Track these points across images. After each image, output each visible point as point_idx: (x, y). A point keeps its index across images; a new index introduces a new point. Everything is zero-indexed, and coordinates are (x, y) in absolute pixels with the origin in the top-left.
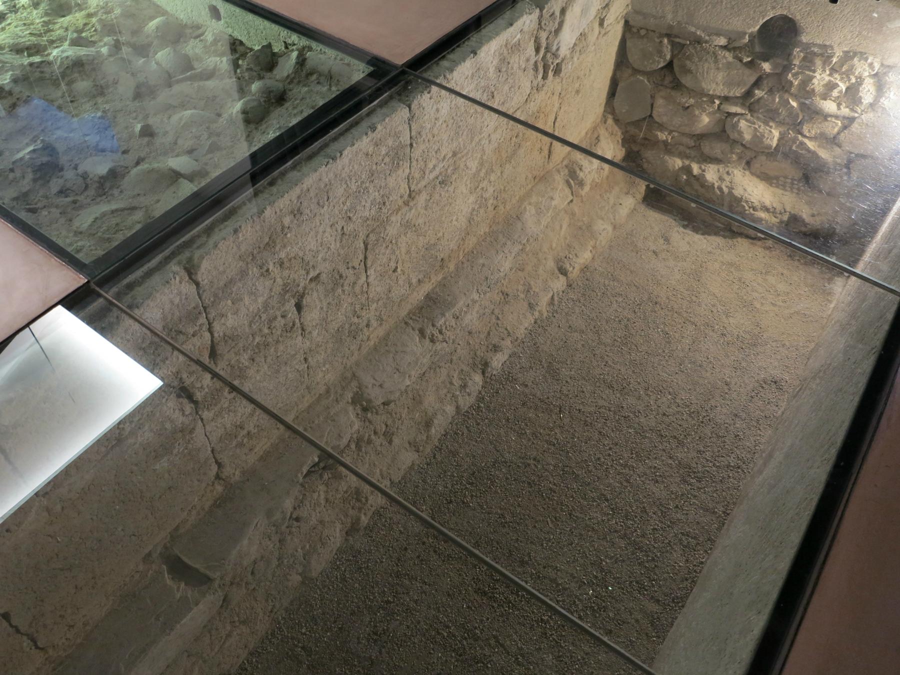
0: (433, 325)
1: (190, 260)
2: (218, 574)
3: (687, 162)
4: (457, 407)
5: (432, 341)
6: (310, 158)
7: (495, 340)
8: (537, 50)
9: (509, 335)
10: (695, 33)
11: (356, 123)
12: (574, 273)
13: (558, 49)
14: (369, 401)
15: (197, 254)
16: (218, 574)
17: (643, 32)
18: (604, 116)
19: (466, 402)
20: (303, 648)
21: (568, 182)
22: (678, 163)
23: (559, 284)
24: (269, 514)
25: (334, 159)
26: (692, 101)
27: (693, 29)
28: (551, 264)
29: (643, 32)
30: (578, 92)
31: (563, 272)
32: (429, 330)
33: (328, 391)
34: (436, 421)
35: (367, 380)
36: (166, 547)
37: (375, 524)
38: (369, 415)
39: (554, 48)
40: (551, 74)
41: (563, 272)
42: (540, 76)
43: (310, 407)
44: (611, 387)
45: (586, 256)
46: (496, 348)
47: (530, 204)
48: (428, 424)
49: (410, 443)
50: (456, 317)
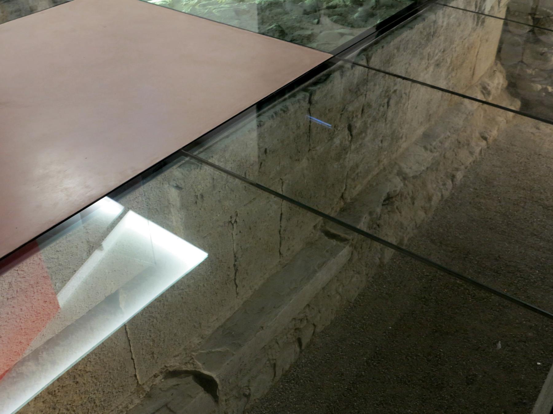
0: (431, 145)
1: (367, 55)
2: (352, 237)
3: (544, 86)
4: (442, 195)
5: (431, 151)
6: (403, 26)
7: (456, 166)
8: (476, 7)
9: (463, 164)
10: (546, 11)
11: (415, 18)
12: (490, 140)
13: (484, 10)
14: (406, 174)
15: (370, 53)
16: (352, 237)
17: (517, 14)
18: (495, 62)
19: (447, 194)
20: (387, 294)
21: (482, 92)
22: (539, 87)
23: (484, 143)
24: (371, 214)
25: (412, 28)
26: (546, 49)
27: (545, 9)
28: (477, 135)
29: (517, 14)
30: (487, 41)
31: (485, 139)
32: (429, 147)
33: (384, 169)
34: (434, 198)
35: (403, 165)
36: (322, 226)
37: (410, 244)
38: (406, 182)
39: (483, 8)
40: (480, 23)
41: (485, 139)
42: (475, 23)
43: (378, 174)
44: (524, 189)
45: (495, 133)
46: (457, 169)
47: (385, 214)
48: (430, 199)
49: (422, 208)
50: (441, 143)
